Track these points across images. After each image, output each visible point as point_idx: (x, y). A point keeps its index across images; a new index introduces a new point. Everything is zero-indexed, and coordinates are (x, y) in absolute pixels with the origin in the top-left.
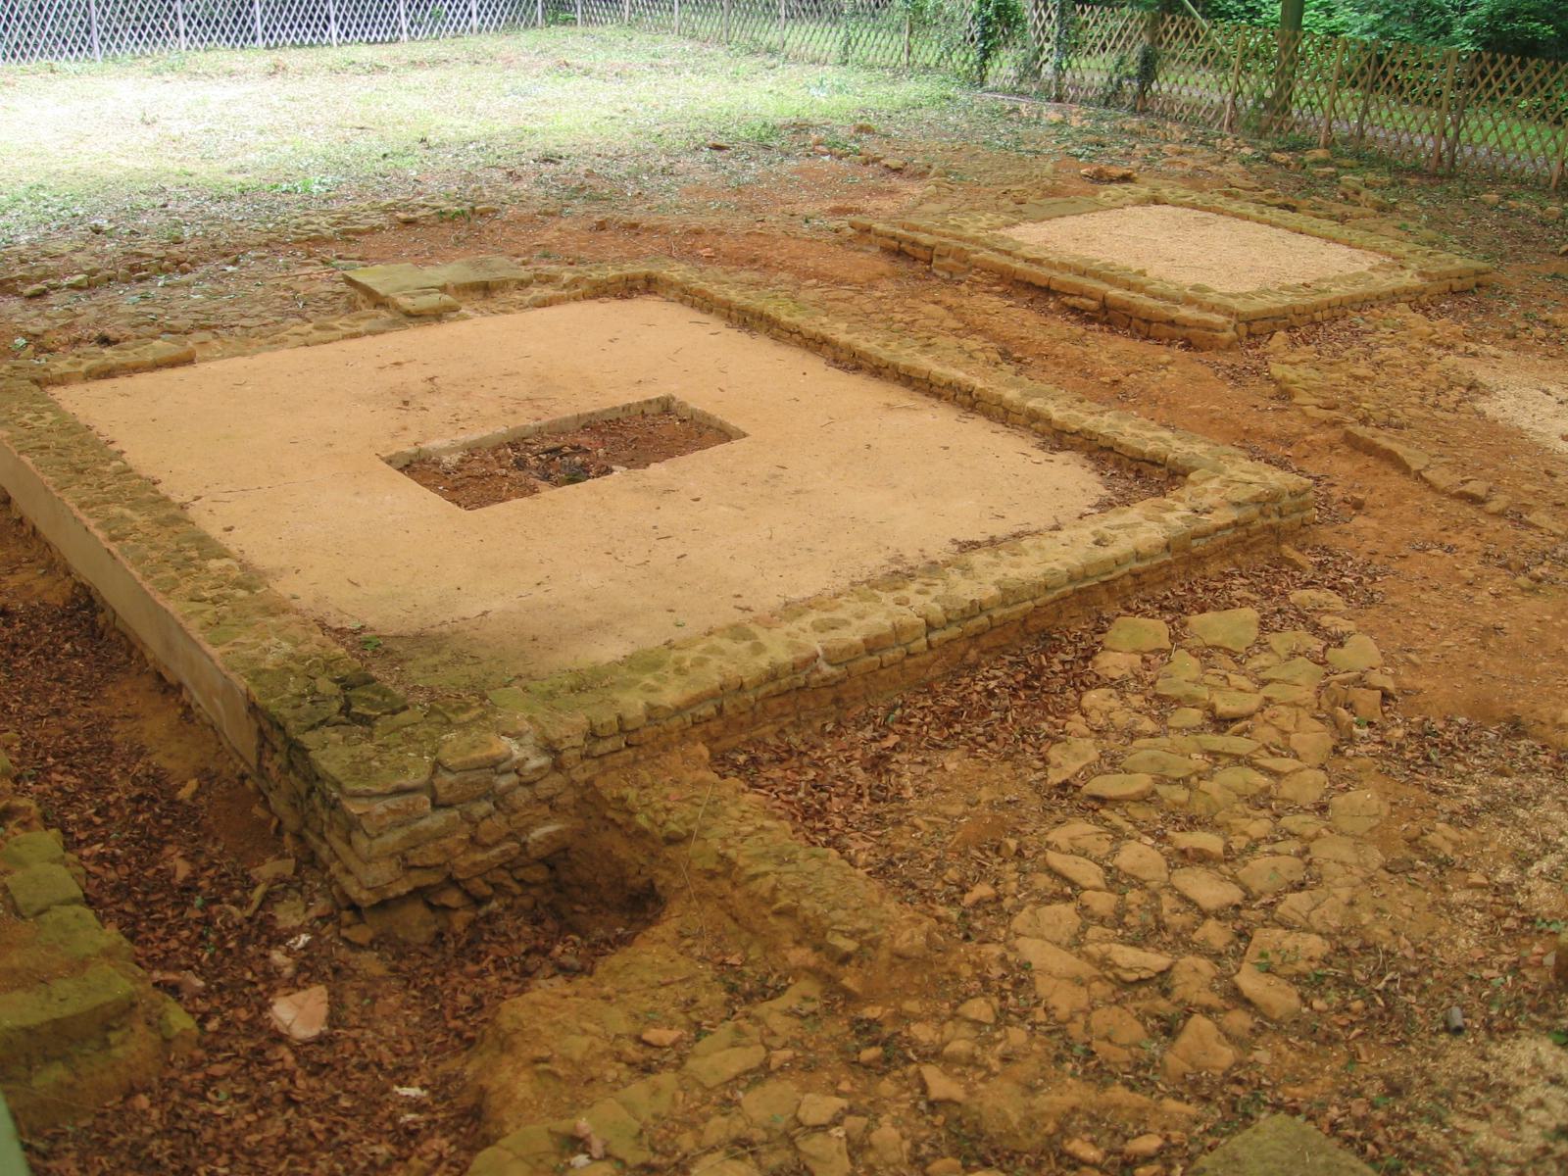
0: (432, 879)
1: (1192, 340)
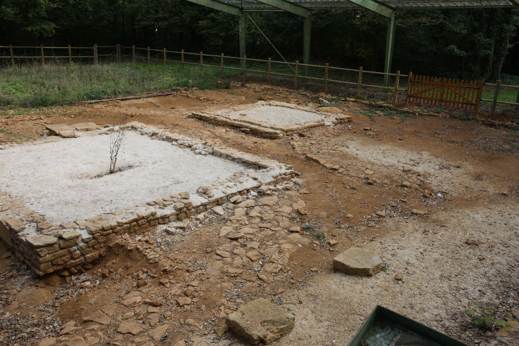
0: (59, 268)
1: (272, 137)
